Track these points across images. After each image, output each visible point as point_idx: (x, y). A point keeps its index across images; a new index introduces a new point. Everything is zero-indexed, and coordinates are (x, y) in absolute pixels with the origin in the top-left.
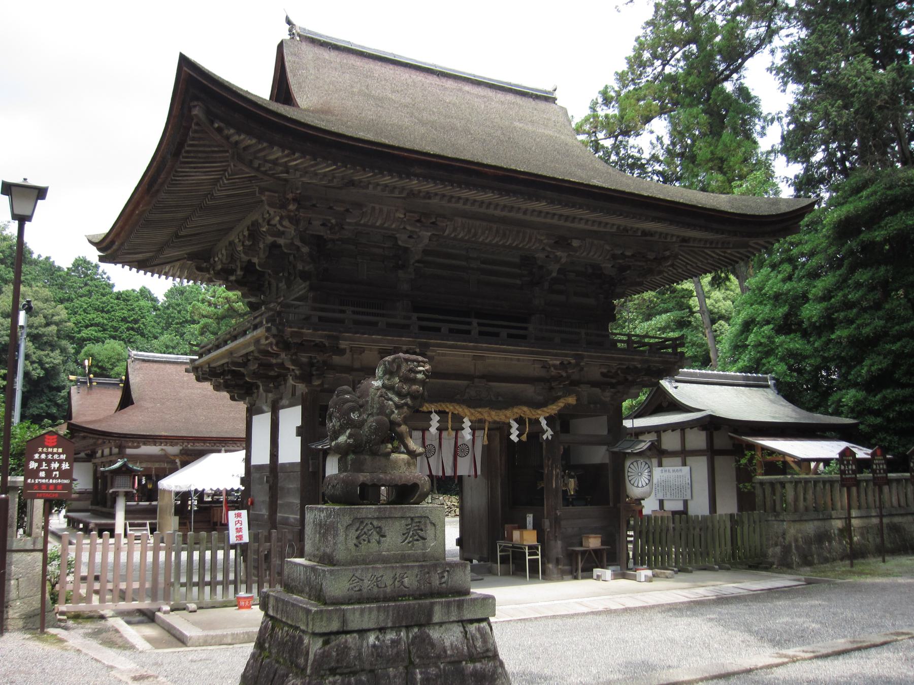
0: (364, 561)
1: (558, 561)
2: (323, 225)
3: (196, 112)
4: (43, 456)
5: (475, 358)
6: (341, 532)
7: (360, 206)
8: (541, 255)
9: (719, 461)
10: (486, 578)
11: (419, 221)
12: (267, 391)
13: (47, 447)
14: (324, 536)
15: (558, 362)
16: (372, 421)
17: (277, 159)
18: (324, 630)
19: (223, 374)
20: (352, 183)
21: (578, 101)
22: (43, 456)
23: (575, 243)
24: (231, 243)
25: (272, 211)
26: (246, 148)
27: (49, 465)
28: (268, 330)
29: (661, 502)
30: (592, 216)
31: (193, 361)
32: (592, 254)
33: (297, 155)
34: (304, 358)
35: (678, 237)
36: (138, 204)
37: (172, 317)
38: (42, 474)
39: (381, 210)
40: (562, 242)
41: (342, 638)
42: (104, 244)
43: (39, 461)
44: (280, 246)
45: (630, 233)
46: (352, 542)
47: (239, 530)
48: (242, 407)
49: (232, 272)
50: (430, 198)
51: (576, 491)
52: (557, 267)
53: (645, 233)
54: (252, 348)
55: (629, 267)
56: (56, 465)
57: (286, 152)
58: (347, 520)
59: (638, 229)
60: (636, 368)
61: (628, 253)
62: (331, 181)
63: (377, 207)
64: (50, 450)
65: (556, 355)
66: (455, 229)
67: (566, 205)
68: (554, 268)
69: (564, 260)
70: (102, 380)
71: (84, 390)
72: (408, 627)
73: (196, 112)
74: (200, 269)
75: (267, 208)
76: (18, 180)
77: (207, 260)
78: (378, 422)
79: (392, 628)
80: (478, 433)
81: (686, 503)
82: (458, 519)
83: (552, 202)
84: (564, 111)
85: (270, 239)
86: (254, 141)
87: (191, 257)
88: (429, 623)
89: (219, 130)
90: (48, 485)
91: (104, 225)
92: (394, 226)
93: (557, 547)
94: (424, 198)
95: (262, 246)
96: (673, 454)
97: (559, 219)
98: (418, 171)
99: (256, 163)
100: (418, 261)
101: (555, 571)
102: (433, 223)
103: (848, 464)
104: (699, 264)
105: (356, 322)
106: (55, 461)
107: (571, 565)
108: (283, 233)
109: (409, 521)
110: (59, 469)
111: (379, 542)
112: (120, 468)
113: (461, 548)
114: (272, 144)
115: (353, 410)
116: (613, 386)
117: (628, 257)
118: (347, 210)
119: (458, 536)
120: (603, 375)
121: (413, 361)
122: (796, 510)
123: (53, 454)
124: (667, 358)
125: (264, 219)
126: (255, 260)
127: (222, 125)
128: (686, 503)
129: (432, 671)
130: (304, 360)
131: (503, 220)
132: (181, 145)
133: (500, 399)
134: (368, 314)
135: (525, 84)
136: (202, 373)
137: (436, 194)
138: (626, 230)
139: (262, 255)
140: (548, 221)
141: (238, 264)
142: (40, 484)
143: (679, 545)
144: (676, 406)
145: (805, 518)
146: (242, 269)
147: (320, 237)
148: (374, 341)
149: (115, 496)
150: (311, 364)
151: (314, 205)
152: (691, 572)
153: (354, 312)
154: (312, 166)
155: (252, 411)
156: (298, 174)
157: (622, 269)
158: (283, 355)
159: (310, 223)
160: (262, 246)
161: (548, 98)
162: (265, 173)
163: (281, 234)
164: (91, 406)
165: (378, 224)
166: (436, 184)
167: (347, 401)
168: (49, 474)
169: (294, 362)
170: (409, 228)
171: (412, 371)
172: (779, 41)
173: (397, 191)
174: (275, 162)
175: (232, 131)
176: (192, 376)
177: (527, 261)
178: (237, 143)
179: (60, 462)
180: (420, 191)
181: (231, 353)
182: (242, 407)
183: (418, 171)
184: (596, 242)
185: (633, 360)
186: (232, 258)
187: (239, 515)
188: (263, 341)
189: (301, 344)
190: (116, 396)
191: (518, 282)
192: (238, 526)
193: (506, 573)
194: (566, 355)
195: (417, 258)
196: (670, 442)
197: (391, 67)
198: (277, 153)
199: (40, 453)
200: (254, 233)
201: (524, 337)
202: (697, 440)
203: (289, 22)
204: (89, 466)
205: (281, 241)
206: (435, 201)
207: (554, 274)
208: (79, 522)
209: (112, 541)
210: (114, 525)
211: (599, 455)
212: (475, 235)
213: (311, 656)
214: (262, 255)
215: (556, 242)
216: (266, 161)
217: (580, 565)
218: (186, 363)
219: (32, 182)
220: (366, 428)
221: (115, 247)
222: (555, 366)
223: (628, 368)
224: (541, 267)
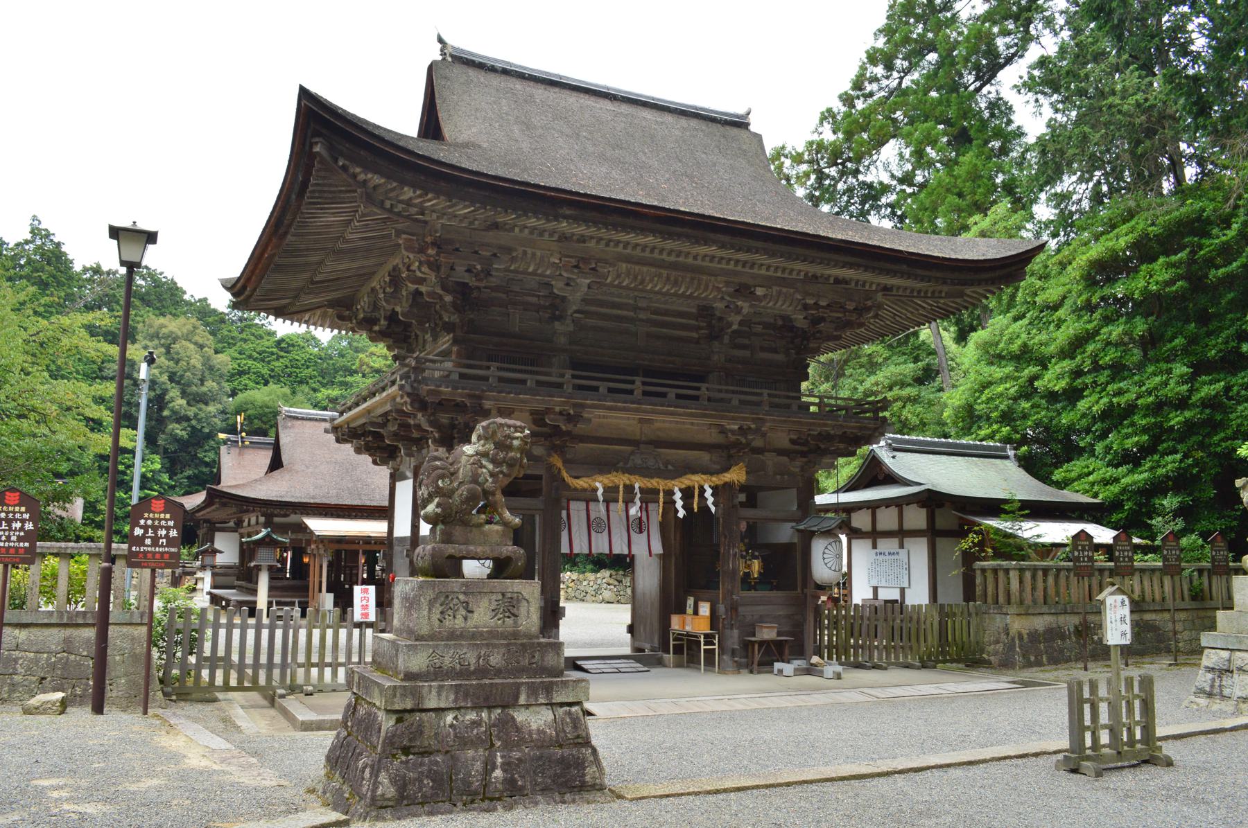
0: (453, 636)
1: (733, 653)
2: (468, 271)
3: (317, 149)
4: (149, 522)
5: (641, 421)
6: (425, 606)
7: (509, 250)
8: (720, 305)
9: (941, 543)
10: (654, 671)
11: (576, 267)
12: (410, 455)
13: (8, 506)
14: (409, 609)
15: (736, 427)
16: (463, 491)
17: (411, 199)
18: (397, 707)
19: (363, 435)
20: (496, 226)
21: (790, 120)
22: (149, 522)
23: (760, 291)
24: (373, 289)
25: (411, 256)
26: (375, 187)
27: (155, 532)
28: (401, 387)
29: (875, 589)
30: (773, 261)
31: (333, 419)
32: (780, 303)
33: (430, 196)
34: (444, 419)
35: (878, 284)
36: (266, 246)
37: (328, 371)
38: (148, 542)
39: (534, 255)
40: (744, 290)
41: (417, 716)
42: (236, 290)
43: (145, 528)
44: (421, 294)
45: (820, 280)
46: (436, 616)
47: (365, 607)
48: (384, 472)
49: (374, 321)
50: (584, 242)
51: (760, 573)
52: (739, 318)
53: (838, 281)
54: (388, 407)
55: (823, 319)
56: (164, 532)
57: (418, 192)
58: (430, 594)
59: (829, 276)
60: (829, 434)
61: (823, 303)
62: (471, 223)
63: (529, 251)
64: (11, 509)
65: (733, 418)
66: (619, 276)
67: (739, 250)
68: (735, 319)
69: (745, 311)
70: (256, 439)
71: (235, 451)
72: (490, 708)
73: (317, 149)
74: (341, 318)
75: (404, 252)
76: (126, 223)
77: (349, 307)
78: (469, 491)
79: (473, 708)
80: (612, 506)
81: (902, 590)
82: (629, 606)
83: (723, 246)
84: (758, 138)
85: (412, 287)
86: (383, 181)
87: (332, 304)
88: (514, 704)
89: (344, 168)
90: (154, 553)
91: (235, 269)
92: (548, 272)
93: (734, 638)
94: (579, 241)
95: (404, 293)
96: (888, 534)
97: (744, 266)
98: (568, 212)
99: (388, 204)
100: (576, 312)
101: (730, 663)
102: (593, 269)
103: (1083, 550)
104: (909, 315)
105: (501, 380)
106: (162, 527)
107: (747, 657)
108: (425, 280)
109: (500, 597)
110: (167, 536)
111: (466, 619)
112: (262, 539)
113: (633, 636)
114: (403, 183)
115: (442, 477)
116: (803, 454)
117: (823, 307)
118: (495, 255)
119: (629, 622)
120: (793, 442)
121: (509, 426)
122: (1021, 602)
123: (160, 520)
124: (859, 425)
125: (404, 264)
126: (398, 309)
127: (347, 163)
128: (902, 590)
129: (516, 754)
130: (445, 421)
131: (674, 266)
132: (305, 184)
133: (670, 467)
134: (520, 371)
135: (713, 108)
136: (345, 434)
137: (592, 238)
138: (815, 277)
139: (404, 304)
140: (723, 266)
141: (382, 312)
142: (145, 553)
143: (887, 638)
144: (892, 479)
145: (1031, 611)
146: (385, 318)
147: (465, 285)
148: (522, 401)
149: (258, 568)
150: (453, 426)
151: (457, 250)
152: (886, 669)
153: (500, 369)
154: (450, 207)
155: (395, 477)
156: (434, 216)
157: (816, 321)
158: (420, 415)
159: (452, 269)
160: (404, 293)
161: (739, 123)
162: (399, 214)
163: (421, 281)
164: (242, 472)
165: (531, 269)
166: (589, 227)
167: (437, 468)
168: (155, 541)
169: (431, 423)
170: (565, 275)
171: (508, 437)
172: (1033, 53)
173: (546, 234)
174: (408, 203)
175: (358, 170)
176: (332, 437)
177: (705, 311)
178: (365, 181)
179: (168, 529)
180: (573, 234)
181: (369, 411)
182: (384, 472)
183: (568, 212)
184: (784, 290)
185: (825, 425)
186: (375, 306)
187: (366, 591)
188: (398, 399)
189: (440, 404)
190: (265, 457)
191: (695, 335)
192: (364, 603)
193: (679, 665)
194: (745, 419)
195: (575, 308)
196: (861, 520)
197: (557, 90)
198: (408, 193)
199: (146, 519)
200: (395, 280)
201: (696, 398)
202: (916, 518)
203: (440, 40)
204: (237, 535)
205: (423, 289)
206: (592, 244)
207: (735, 327)
208: (222, 599)
209: (252, 621)
210: (255, 602)
211: (785, 533)
212: (642, 282)
213: (383, 734)
214: (404, 304)
215: (737, 291)
216: (400, 202)
217: (759, 657)
218: (324, 420)
219: (142, 226)
220: (456, 496)
221: (247, 293)
222: (733, 432)
223: (820, 434)
224: (721, 319)
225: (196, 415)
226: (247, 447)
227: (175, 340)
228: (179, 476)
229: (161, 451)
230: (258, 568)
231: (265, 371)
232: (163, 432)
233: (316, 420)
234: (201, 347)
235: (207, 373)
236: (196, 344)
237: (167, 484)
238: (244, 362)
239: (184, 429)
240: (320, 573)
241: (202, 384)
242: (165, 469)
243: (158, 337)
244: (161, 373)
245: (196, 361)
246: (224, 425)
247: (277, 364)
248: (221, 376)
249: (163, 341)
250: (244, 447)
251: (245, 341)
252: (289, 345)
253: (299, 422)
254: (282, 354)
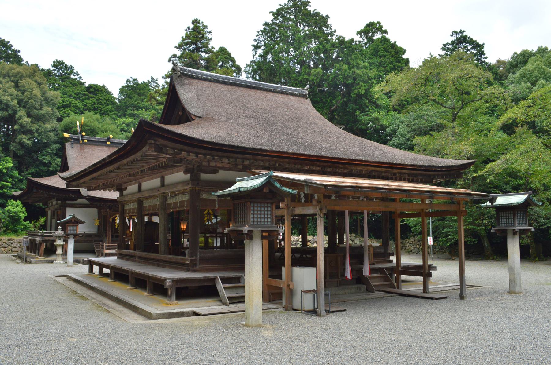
225: (37, 130)
226: (86, 144)
227: (21, 78)
228: (26, 173)
229: (12, 154)
230: (250, 235)
231: (80, 105)
232: (14, 142)
233: (210, 81)
234: (40, 84)
235: (43, 103)
236: (36, 82)
237: (17, 178)
238: (66, 99)
239: (29, 139)
240: (163, 237)
241: (41, 109)
242: (16, 168)
243: (9, 76)
244: (12, 99)
245: (37, 92)
246: (56, 138)
247: (88, 101)
248: (54, 105)
249: (12, 78)
250: (84, 143)
251: (66, 86)
252: (96, 90)
253: (195, 81)
254: (91, 95)
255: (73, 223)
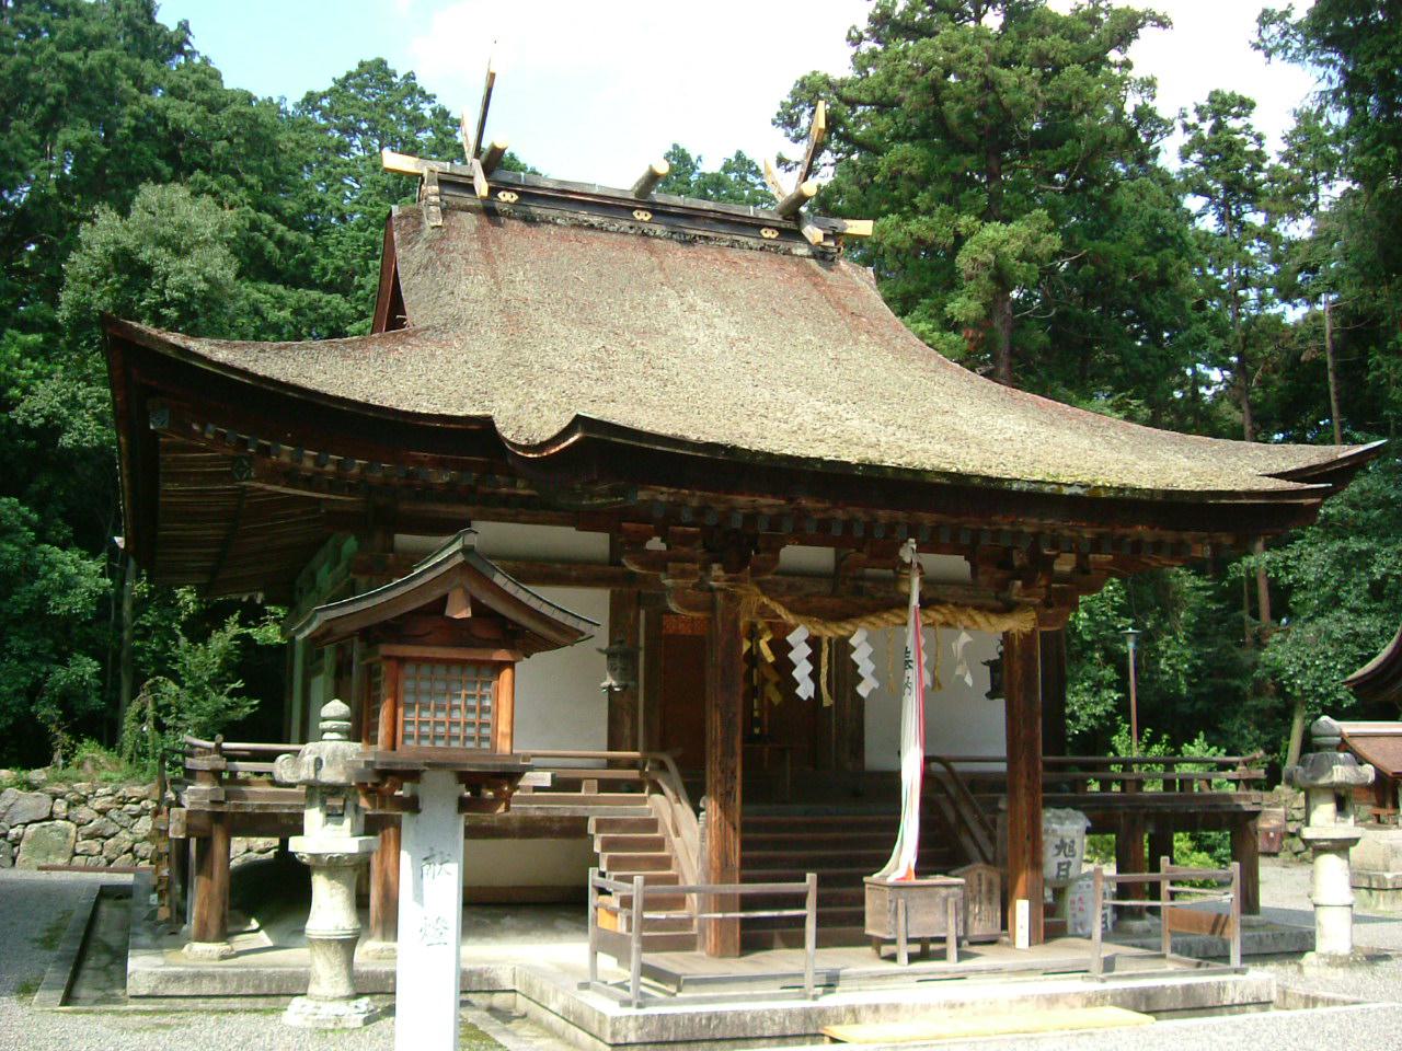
255: (459, 634)
